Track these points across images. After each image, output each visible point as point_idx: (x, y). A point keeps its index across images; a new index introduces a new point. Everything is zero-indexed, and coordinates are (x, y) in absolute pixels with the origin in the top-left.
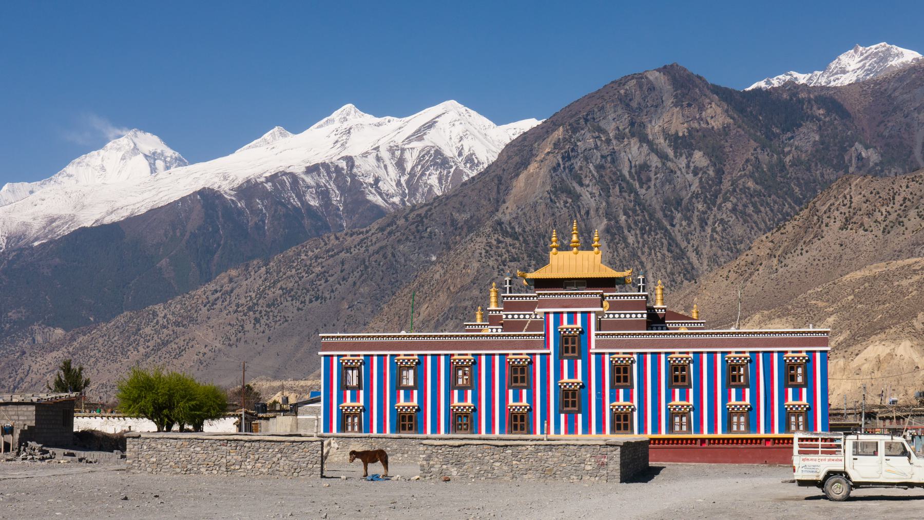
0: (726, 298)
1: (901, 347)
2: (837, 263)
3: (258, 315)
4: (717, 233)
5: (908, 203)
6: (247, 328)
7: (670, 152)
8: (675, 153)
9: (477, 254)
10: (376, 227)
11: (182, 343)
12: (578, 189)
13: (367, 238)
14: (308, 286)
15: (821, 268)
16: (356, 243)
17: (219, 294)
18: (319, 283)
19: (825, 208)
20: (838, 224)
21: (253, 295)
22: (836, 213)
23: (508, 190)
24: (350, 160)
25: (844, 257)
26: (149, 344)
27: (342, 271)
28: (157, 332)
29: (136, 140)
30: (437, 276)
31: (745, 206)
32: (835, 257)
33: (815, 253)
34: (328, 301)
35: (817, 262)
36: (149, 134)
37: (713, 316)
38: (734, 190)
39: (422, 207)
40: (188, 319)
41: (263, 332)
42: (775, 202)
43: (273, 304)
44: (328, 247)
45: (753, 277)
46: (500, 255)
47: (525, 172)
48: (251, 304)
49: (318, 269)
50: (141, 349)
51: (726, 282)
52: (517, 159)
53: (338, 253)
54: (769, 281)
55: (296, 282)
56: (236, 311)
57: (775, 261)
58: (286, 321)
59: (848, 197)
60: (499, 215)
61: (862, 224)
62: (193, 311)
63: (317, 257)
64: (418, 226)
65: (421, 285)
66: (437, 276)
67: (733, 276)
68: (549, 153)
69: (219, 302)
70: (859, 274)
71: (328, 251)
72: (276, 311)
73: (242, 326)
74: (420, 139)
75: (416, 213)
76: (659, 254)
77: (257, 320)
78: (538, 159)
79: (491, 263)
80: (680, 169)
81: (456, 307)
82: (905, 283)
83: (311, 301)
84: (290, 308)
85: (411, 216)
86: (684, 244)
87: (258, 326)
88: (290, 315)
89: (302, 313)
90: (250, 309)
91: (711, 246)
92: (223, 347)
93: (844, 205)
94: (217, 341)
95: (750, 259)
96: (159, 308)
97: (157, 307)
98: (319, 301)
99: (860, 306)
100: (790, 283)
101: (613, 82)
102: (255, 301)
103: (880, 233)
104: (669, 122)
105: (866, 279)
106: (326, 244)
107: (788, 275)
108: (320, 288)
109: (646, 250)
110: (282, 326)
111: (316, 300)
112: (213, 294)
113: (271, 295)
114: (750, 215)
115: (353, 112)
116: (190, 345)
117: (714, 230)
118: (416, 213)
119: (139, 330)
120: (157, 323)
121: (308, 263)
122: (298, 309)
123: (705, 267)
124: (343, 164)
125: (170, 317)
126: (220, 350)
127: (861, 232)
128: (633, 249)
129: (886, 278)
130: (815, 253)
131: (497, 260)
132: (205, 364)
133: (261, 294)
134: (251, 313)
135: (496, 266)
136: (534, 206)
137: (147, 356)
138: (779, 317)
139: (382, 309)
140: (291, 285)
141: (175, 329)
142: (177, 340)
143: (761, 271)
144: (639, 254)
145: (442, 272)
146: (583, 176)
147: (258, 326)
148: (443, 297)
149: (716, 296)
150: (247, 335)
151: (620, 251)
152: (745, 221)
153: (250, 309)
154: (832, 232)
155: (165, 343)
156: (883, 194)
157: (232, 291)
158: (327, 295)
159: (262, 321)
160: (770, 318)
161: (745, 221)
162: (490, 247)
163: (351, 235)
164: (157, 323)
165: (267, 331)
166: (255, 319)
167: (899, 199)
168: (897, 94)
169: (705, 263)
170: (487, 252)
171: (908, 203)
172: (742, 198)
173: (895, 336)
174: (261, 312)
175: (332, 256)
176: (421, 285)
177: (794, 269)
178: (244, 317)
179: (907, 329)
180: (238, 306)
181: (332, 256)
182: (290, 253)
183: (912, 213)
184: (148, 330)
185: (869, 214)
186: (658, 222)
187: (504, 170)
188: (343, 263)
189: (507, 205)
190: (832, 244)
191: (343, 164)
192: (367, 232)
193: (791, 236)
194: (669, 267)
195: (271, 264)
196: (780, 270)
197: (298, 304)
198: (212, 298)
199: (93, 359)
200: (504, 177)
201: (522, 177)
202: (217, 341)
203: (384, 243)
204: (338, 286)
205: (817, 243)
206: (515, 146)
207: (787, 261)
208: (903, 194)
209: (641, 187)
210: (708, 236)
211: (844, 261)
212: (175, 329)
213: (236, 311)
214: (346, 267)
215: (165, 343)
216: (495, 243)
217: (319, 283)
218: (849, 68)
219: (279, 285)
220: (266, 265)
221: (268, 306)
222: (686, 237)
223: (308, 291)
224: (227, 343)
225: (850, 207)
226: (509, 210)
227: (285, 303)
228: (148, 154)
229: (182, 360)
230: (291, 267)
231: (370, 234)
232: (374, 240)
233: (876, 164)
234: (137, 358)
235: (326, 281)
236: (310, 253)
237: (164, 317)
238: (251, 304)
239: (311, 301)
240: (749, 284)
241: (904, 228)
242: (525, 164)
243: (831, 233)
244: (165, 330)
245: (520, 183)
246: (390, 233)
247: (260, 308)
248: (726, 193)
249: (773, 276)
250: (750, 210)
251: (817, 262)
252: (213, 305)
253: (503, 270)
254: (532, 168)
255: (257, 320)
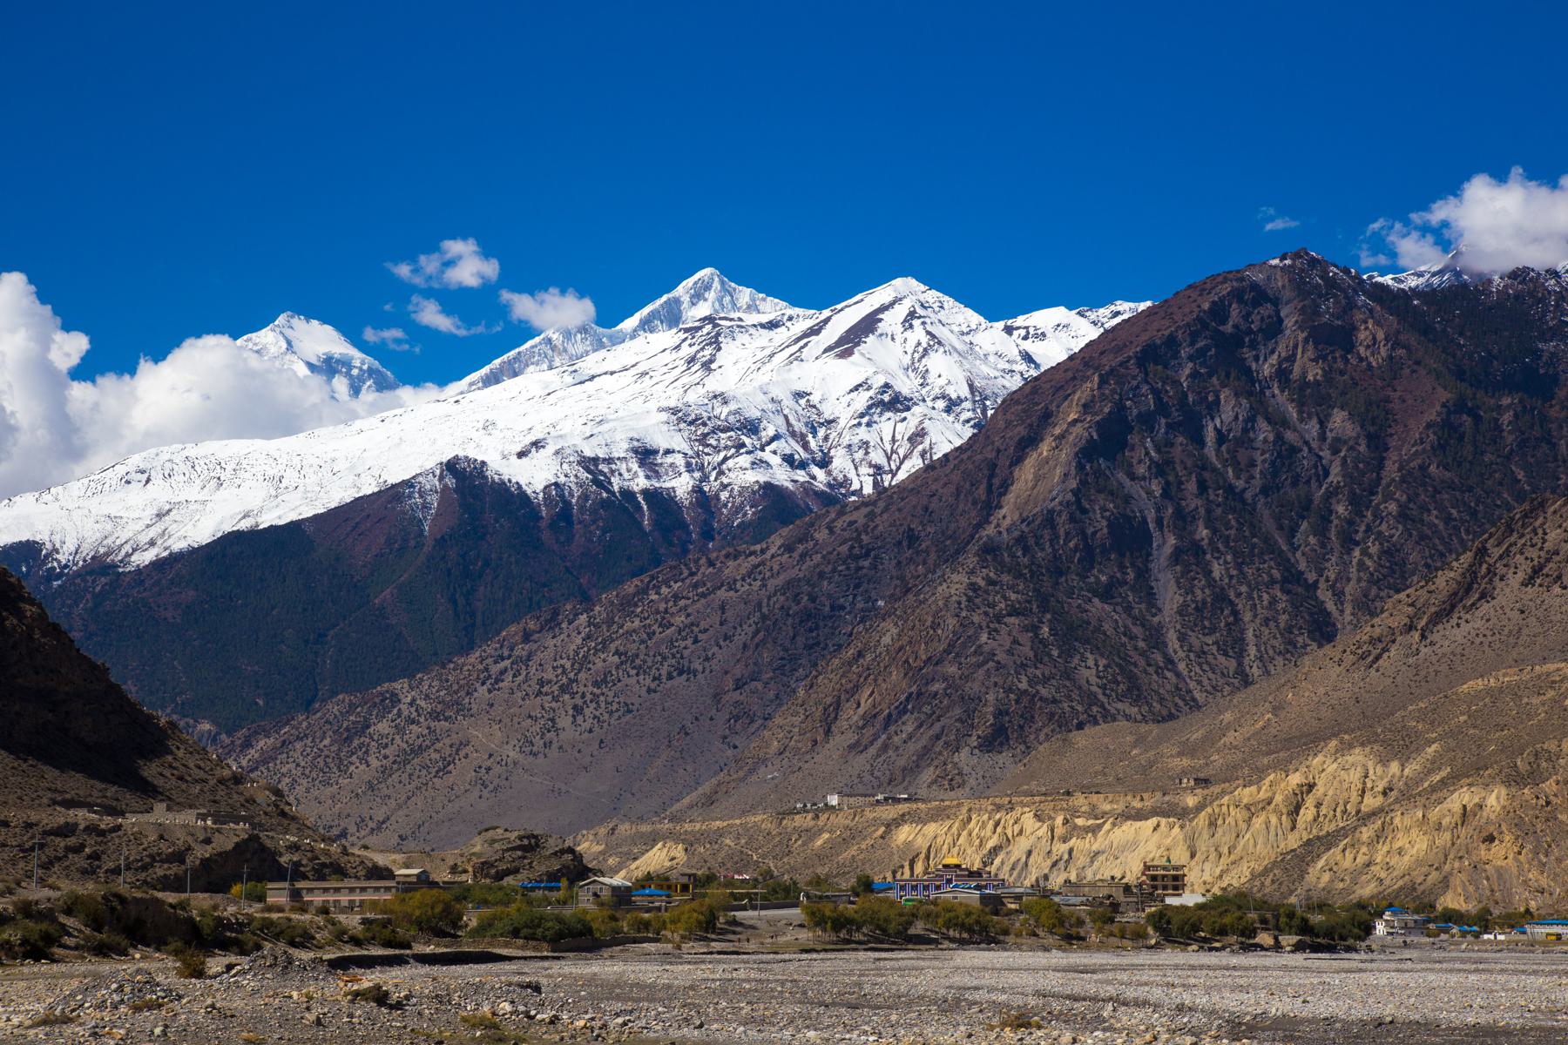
0: (1335, 695)
1: (1494, 795)
2: (1512, 640)
3: (580, 702)
4: (1370, 556)
6: (561, 723)
8: (1300, 412)
10: (778, 543)
11: (448, 751)
13: (763, 563)
14: (664, 649)
15: (1486, 648)
16: (743, 571)
17: (507, 663)
18: (683, 644)
20: (1521, 576)
21: (568, 665)
22: (1519, 558)
23: (1006, 486)
25: (1525, 631)
26: (387, 751)
27: (721, 624)
28: (400, 730)
29: (288, 332)
30: (887, 640)
32: (1510, 632)
33: (1479, 624)
34: (700, 676)
35: (1481, 638)
36: (315, 323)
37: (1315, 723)
39: (857, 508)
40: (452, 707)
41: (591, 731)
43: (604, 681)
44: (696, 579)
45: (1381, 662)
47: (1035, 455)
48: (565, 680)
49: (680, 620)
50: (375, 763)
51: (1338, 669)
52: (1021, 431)
53: (713, 592)
54: (1404, 668)
55: (643, 642)
57: (1417, 635)
58: (630, 711)
59: (1540, 531)
60: (990, 530)
62: (462, 693)
63: (676, 597)
64: (852, 547)
65: (860, 654)
66: (887, 640)
68: (1075, 421)
69: (509, 677)
70: (1480, 684)
71: (696, 586)
72: (611, 694)
73: (552, 720)
75: (847, 518)
76: (1265, 596)
77: (578, 710)
79: (976, 619)
80: (1306, 443)
81: (920, 694)
83: (670, 677)
84: (635, 686)
86: (1311, 577)
87: (580, 719)
88: (636, 701)
89: (657, 696)
90: (563, 689)
91: (1359, 580)
92: (521, 757)
93: (1533, 546)
94: (510, 747)
96: (400, 686)
97: (397, 685)
98: (685, 676)
99: (1472, 731)
100: (1437, 672)
101: (1190, 287)
102: (572, 675)
104: (1291, 358)
105: (1489, 691)
106: (692, 574)
107: (1434, 659)
108: (686, 653)
110: (624, 720)
111: (680, 674)
112: (496, 662)
113: (600, 664)
115: (716, 285)
116: (462, 753)
118: (847, 518)
119: (368, 727)
120: (399, 714)
121: (662, 606)
122: (649, 691)
123: (1348, 618)
125: (423, 704)
126: (515, 764)
128: (1223, 589)
129: (1515, 692)
130: (1479, 624)
131: (986, 614)
132: (491, 787)
133: (583, 663)
134: (567, 697)
135: (984, 624)
136: (1049, 519)
137: (385, 772)
138: (1362, 745)
139: (794, 691)
140: (635, 646)
141: (432, 724)
142: (438, 746)
144: (1232, 597)
145: (895, 631)
146: (1135, 461)
147: (580, 719)
148: (895, 675)
149: (1322, 690)
150: (563, 735)
151: (1199, 592)
154: (1510, 589)
155: (418, 751)
157: (529, 658)
158: (697, 665)
159: (587, 711)
160: (1351, 746)
162: (975, 591)
163: (736, 558)
164: (399, 714)
165: (596, 729)
166: (575, 707)
169: (1348, 610)
170: (969, 600)
172: (1417, 495)
173: (1488, 780)
174: (583, 696)
175: (703, 595)
176: (860, 654)
177: (1444, 650)
178: (554, 705)
180: (541, 683)
181: (703, 595)
182: (630, 587)
184: (383, 727)
186: (1267, 539)
187: (999, 451)
188: (723, 608)
189: (1004, 511)
190: (1507, 610)
192: (763, 551)
193: (1443, 596)
194: (1283, 618)
195: (597, 608)
196: (1423, 650)
197: (648, 681)
198: (495, 669)
199: (287, 780)
200: (1000, 463)
201: (1030, 463)
202: (510, 747)
203: (793, 573)
204: (715, 649)
205: (1485, 607)
206: (1018, 402)
207: (1435, 637)
209: (1238, 478)
210: (1355, 561)
211: (1524, 637)
212: (432, 724)
213: (539, 693)
214: (729, 614)
215: (418, 751)
216: (982, 583)
217: (683, 644)
219: (613, 647)
220: (588, 610)
221: (596, 684)
222: (1318, 563)
223: (665, 658)
224: (527, 750)
225: (1541, 549)
226: (1008, 521)
227: (626, 680)
228: (314, 361)
229: (449, 779)
230: (632, 614)
231: (768, 555)
232: (776, 568)
234: (366, 778)
235: (696, 641)
237: (411, 704)
238: (565, 680)
239: (670, 677)
240: (1373, 671)
242: (1029, 442)
243: (1507, 590)
244: (414, 727)
245: (1026, 473)
246: (803, 556)
247: (582, 689)
248: (1389, 485)
249: (1411, 660)
251: (1481, 638)
252: (497, 682)
253: (996, 630)
254: (1045, 448)
255: (578, 710)
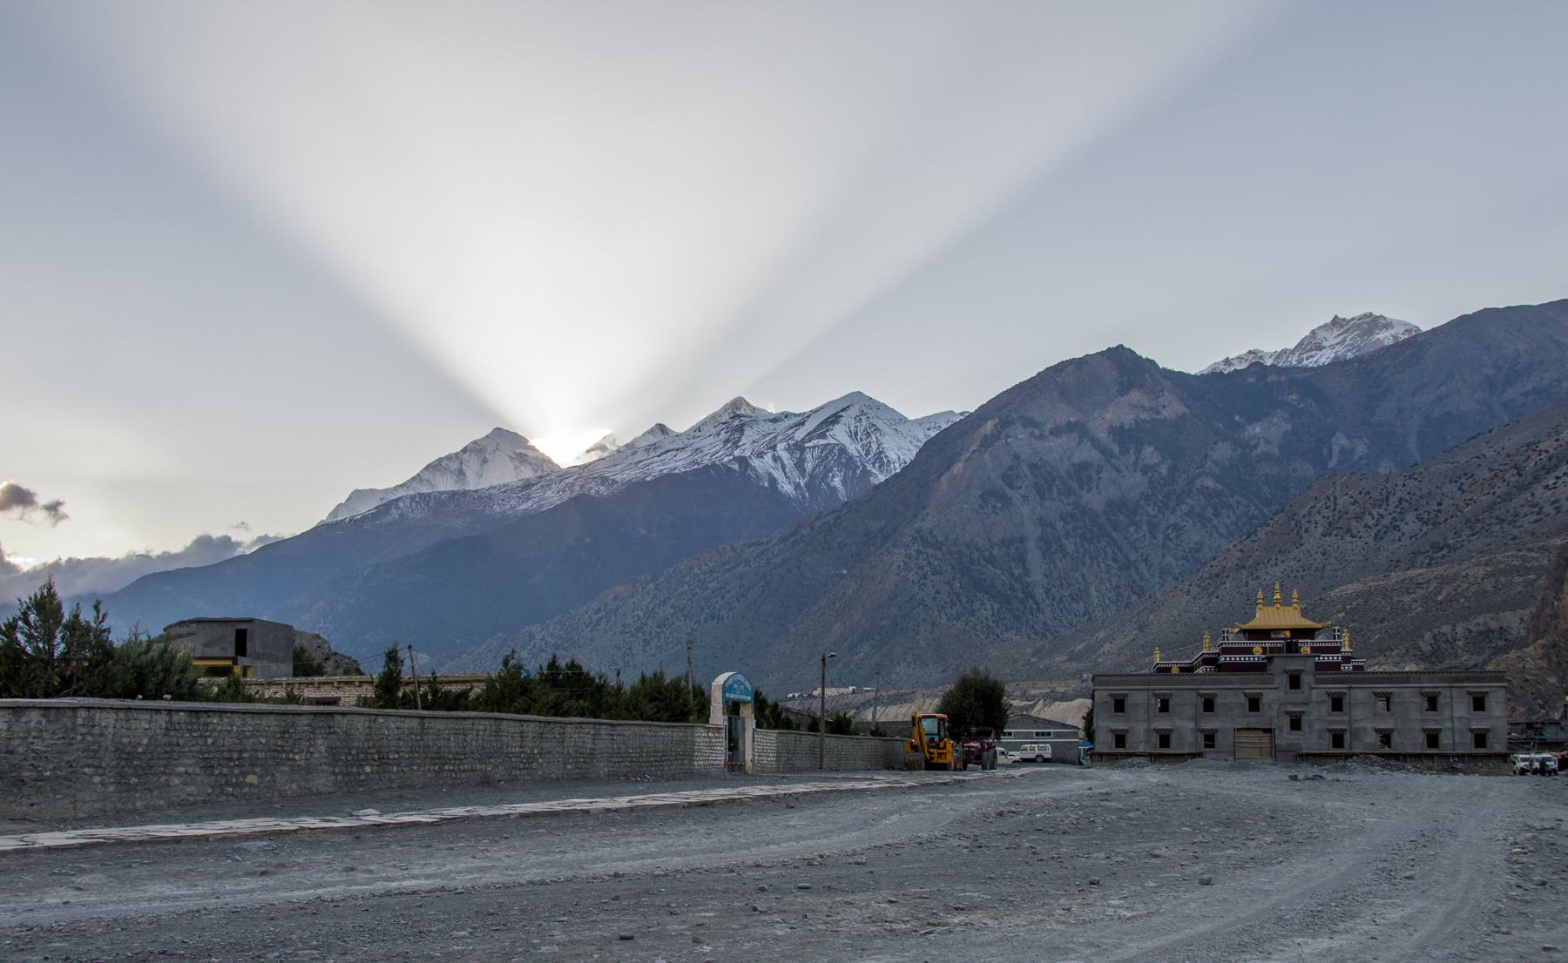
3: (647, 637)
5: (1405, 504)
7: (1116, 448)
9: (894, 567)
12: (1009, 492)
19: (1304, 511)
20: (1320, 529)
22: (1318, 517)
24: (743, 461)
31: (1203, 508)
38: (1190, 491)
42: (1238, 503)
46: (921, 568)
49: (714, 585)
56: (623, 632)
61: (1349, 531)
63: (711, 571)
66: (849, 592)
67: (1194, 590)
74: (823, 436)
77: (647, 643)
78: (962, 458)
79: (911, 577)
82: (1407, 599)
85: (818, 524)
95: (1215, 570)
103: (1370, 540)
109: (1088, 560)
114: (1209, 520)
117: (1167, 537)
124: (735, 466)
127: (1348, 538)
143: (1228, 585)
149: (1175, 613)
152: (1204, 526)
153: (638, 629)
156: (1375, 494)
158: (723, 613)
161: (1204, 526)
167: (1394, 500)
168: (1387, 374)
171: (1405, 504)
179: (1412, 652)
180: (624, 626)
183: (1410, 516)
185: (1358, 518)
191: (735, 466)
198: (595, 618)
207: (1260, 573)
208: (1399, 494)
213: (623, 632)
218: (1325, 344)
221: (659, 626)
233: (1361, 458)
236: (704, 568)
241: (1398, 534)
250: (1209, 513)
255: (647, 643)
